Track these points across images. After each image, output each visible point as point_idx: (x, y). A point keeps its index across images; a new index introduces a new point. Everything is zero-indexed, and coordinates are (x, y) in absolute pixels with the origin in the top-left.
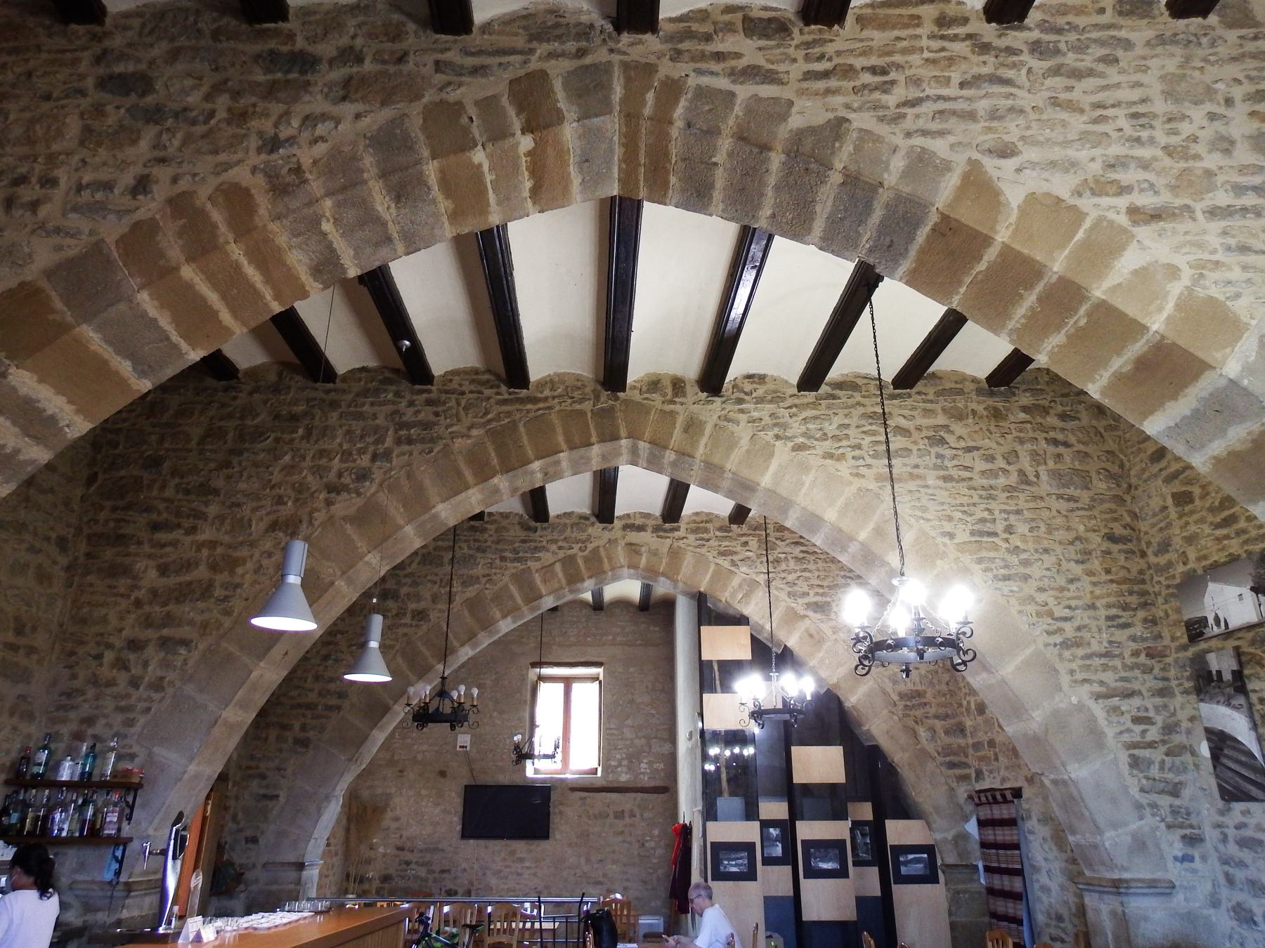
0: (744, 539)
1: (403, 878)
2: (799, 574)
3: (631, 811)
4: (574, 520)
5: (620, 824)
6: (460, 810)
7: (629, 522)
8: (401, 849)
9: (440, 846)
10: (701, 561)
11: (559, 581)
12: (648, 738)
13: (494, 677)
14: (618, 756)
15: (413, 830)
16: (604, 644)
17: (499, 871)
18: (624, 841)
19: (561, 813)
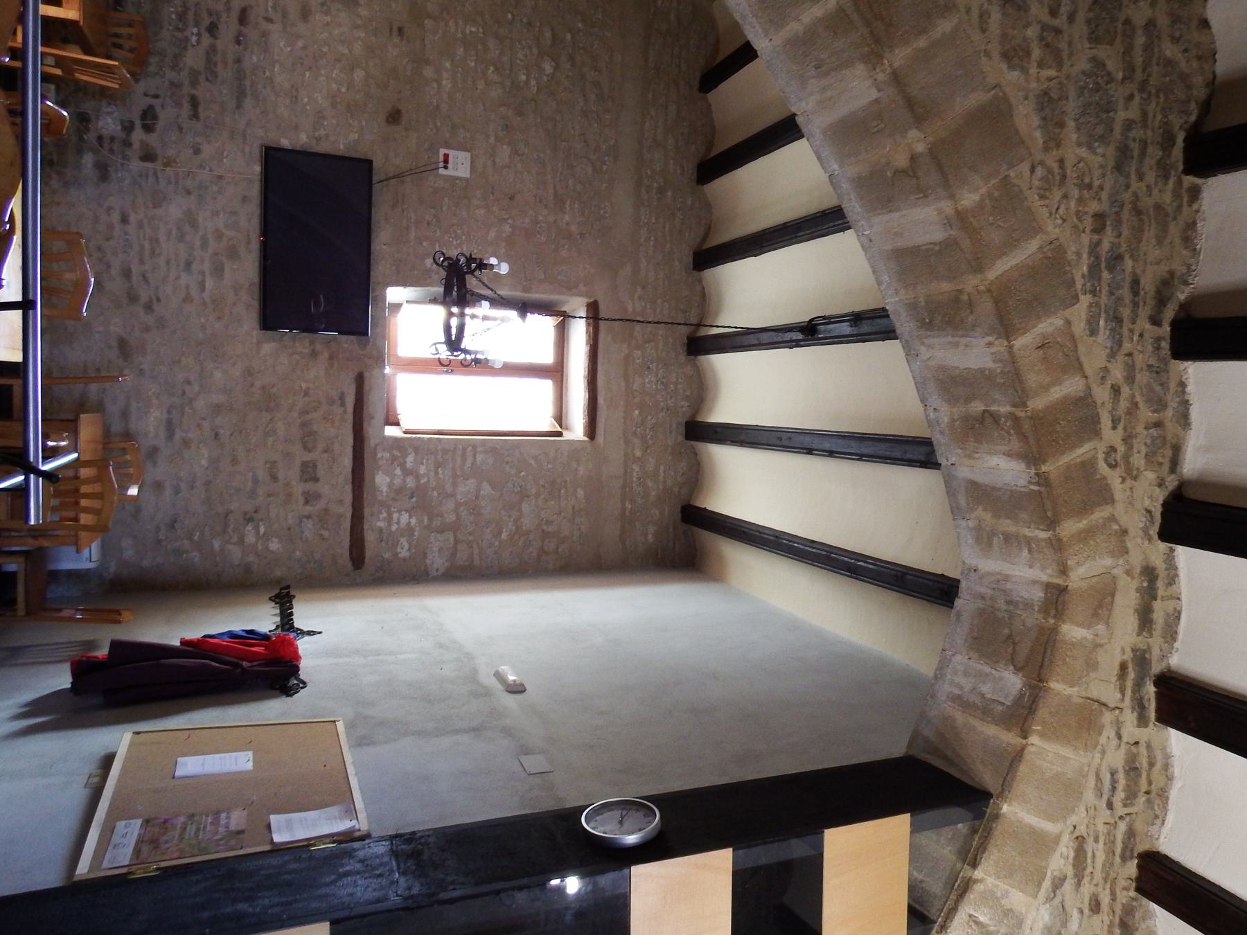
0: (1105, 899)
1: (182, 16)
3: (318, 496)
4: (1171, 428)
5: (290, 473)
6: (324, 147)
7: (1160, 584)
8: (243, 18)
9: (248, 102)
10: (1065, 792)
11: (1046, 388)
12: (455, 528)
13: (574, 228)
14: (422, 470)
15: (280, 44)
16: (627, 442)
17: (194, 224)
18: (256, 481)
19: (314, 354)
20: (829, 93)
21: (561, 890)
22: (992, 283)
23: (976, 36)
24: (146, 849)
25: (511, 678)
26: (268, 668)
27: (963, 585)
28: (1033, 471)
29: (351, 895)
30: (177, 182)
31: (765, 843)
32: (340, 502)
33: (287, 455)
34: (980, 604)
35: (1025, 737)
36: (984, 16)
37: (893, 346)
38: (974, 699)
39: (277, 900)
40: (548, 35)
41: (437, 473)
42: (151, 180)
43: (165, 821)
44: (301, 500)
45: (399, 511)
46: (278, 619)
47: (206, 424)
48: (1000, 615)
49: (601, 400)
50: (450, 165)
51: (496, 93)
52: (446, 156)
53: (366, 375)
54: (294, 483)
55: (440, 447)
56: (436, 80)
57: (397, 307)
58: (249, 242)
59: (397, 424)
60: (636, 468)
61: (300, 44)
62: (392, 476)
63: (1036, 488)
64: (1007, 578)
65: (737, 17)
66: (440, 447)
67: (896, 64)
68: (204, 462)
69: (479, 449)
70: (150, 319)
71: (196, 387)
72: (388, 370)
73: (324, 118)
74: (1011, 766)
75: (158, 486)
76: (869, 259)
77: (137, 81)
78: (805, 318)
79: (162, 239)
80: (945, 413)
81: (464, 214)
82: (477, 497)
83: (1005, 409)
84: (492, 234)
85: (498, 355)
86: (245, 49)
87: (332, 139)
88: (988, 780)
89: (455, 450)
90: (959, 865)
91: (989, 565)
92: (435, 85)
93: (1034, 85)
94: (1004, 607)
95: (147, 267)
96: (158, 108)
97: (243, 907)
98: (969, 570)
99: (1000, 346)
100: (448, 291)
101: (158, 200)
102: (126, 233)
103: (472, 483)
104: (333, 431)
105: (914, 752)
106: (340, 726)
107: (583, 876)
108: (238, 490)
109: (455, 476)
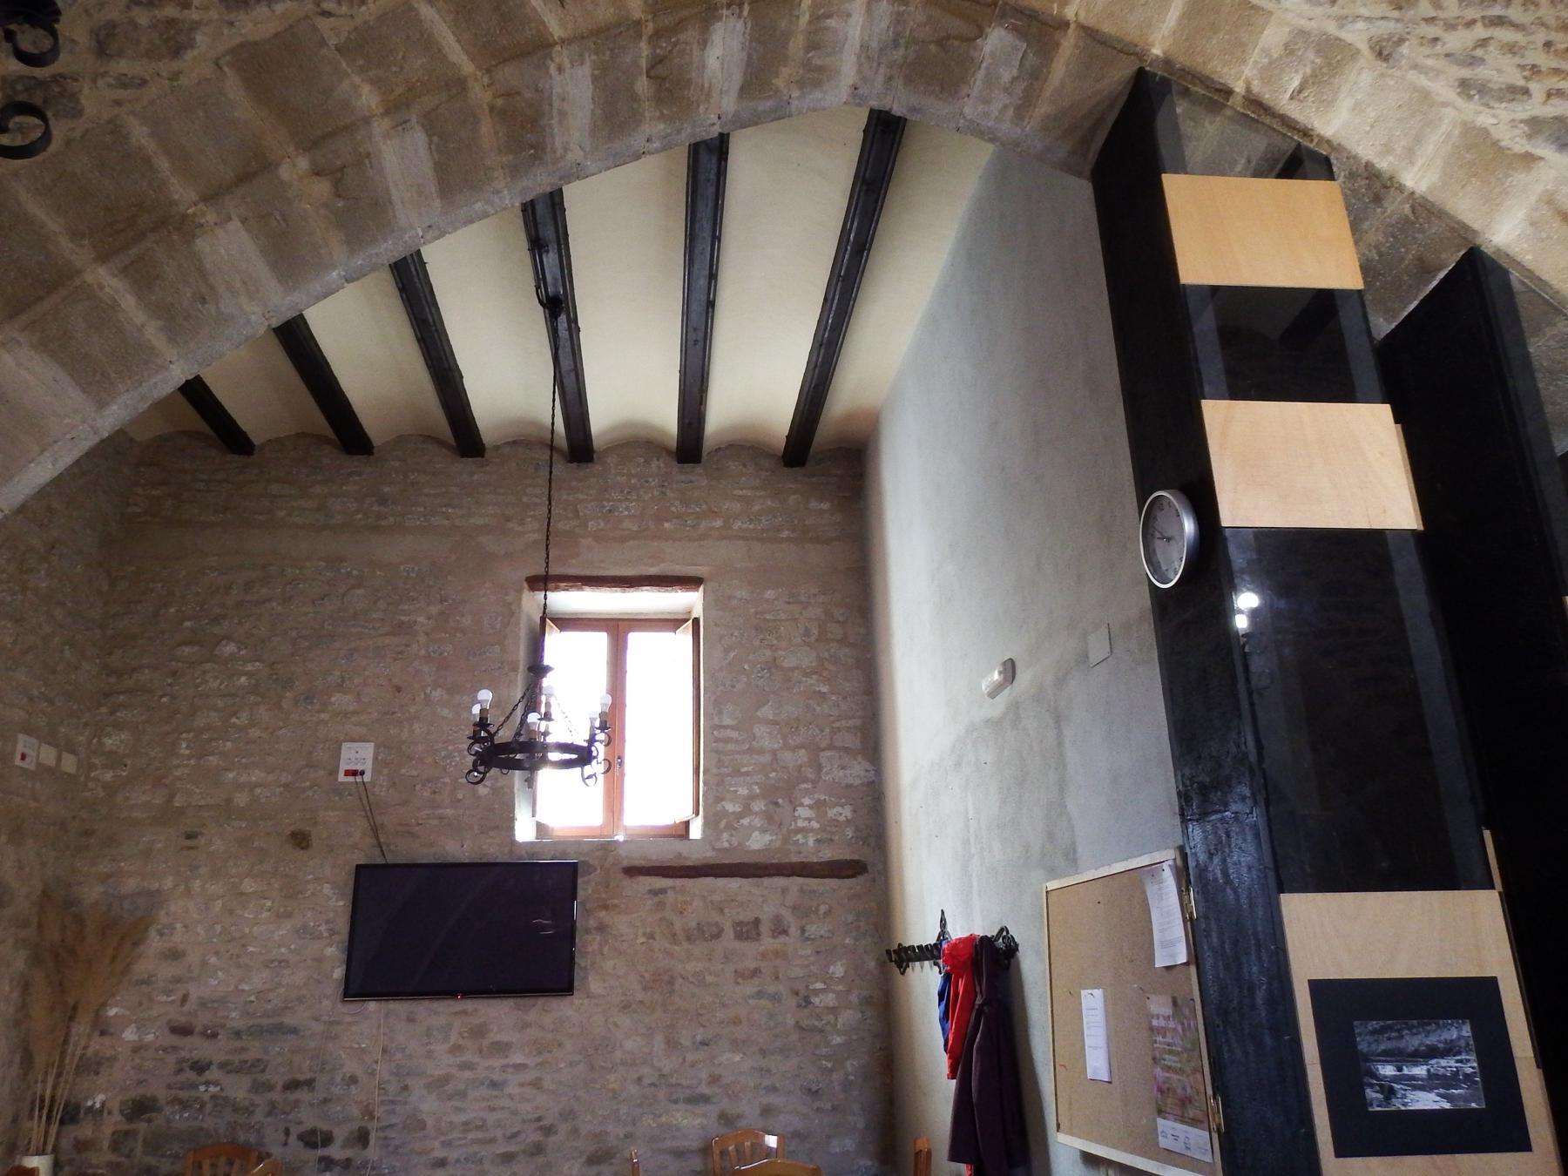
1: (185, 1105)
2: (1480, 32)
3: (778, 919)
5: (749, 953)
6: (343, 926)
8: (183, 1031)
9: (289, 1020)
12: (814, 750)
14: (743, 791)
15: (215, 984)
16: (704, 537)
17: (445, 1080)
18: (760, 995)
19: (602, 928)
20: (238, 285)
21: (1254, 614)
22: (479, 67)
23: (152, 91)
24: (1191, 1113)
25: (996, 676)
26: (984, 974)
27: (875, 104)
28: (725, 12)
29: (1250, 868)
30: (393, 1102)
31: (1197, 360)
32: (784, 891)
33: (727, 958)
34: (898, 82)
35: (1067, 24)
36: (123, 82)
37: (573, 196)
38: (1020, 88)
39: (1253, 958)
40: (187, 650)
41: (747, 774)
42: (392, 1134)
43: (1161, 1091)
44: (783, 938)
45: (796, 819)
46: (927, 963)
47: (690, 1057)
48: (912, 56)
49: (653, 571)
50: (359, 768)
51: (263, 713)
52: (347, 773)
53: (625, 863)
54: (762, 948)
55: (715, 771)
56: (251, 790)
57: (541, 828)
58: (465, 1013)
59: (687, 824)
60: (737, 525)
61: (213, 960)
62: (752, 828)
63: (746, 8)
64: (864, 47)
65: (145, 406)
66: (715, 771)
67: (194, 196)
68: (737, 1058)
69: (716, 720)
70: (564, 1128)
71: (646, 1070)
72: (620, 838)
73: (305, 927)
74: (1103, 43)
75: (767, 1111)
76: (456, 229)
77: (269, 1155)
78: (539, 313)
79: (463, 1118)
80: (652, 128)
81: (420, 748)
82: (775, 723)
83: (644, 49)
84: (445, 712)
85: (596, 700)
86: (223, 1026)
87: (331, 915)
88: (1119, 74)
89: (718, 752)
90: (1229, 112)
91: (848, 68)
92: (258, 791)
93: (214, 14)
94: (901, 51)
95: (499, 1134)
96: (301, 1129)
97: (1260, 997)
98: (854, 95)
99: (561, 55)
100: (517, 765)
101: (416, 1124)
102: (458, 1161)
103: (759, 730)
104: (697, 903)
105: (1088, 169)
106: (1052, 885)
107: (1233, 588)
108: (771, 1016)
109: (751, 751)
